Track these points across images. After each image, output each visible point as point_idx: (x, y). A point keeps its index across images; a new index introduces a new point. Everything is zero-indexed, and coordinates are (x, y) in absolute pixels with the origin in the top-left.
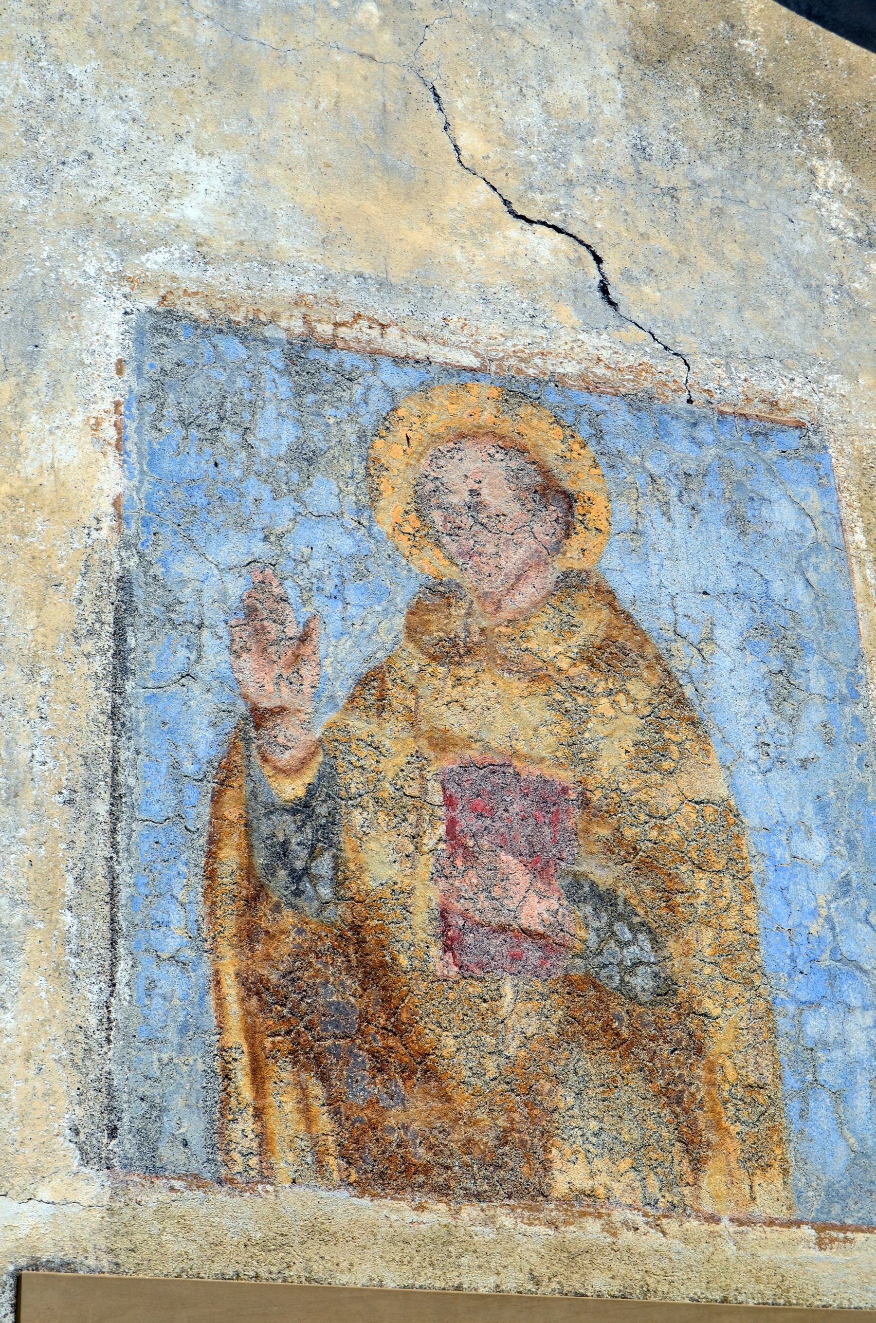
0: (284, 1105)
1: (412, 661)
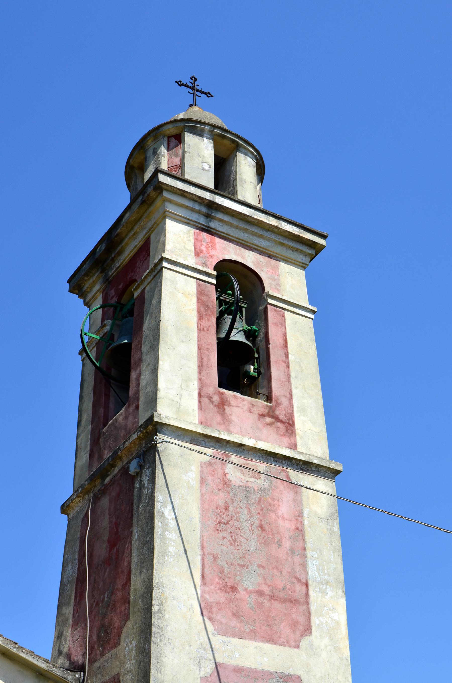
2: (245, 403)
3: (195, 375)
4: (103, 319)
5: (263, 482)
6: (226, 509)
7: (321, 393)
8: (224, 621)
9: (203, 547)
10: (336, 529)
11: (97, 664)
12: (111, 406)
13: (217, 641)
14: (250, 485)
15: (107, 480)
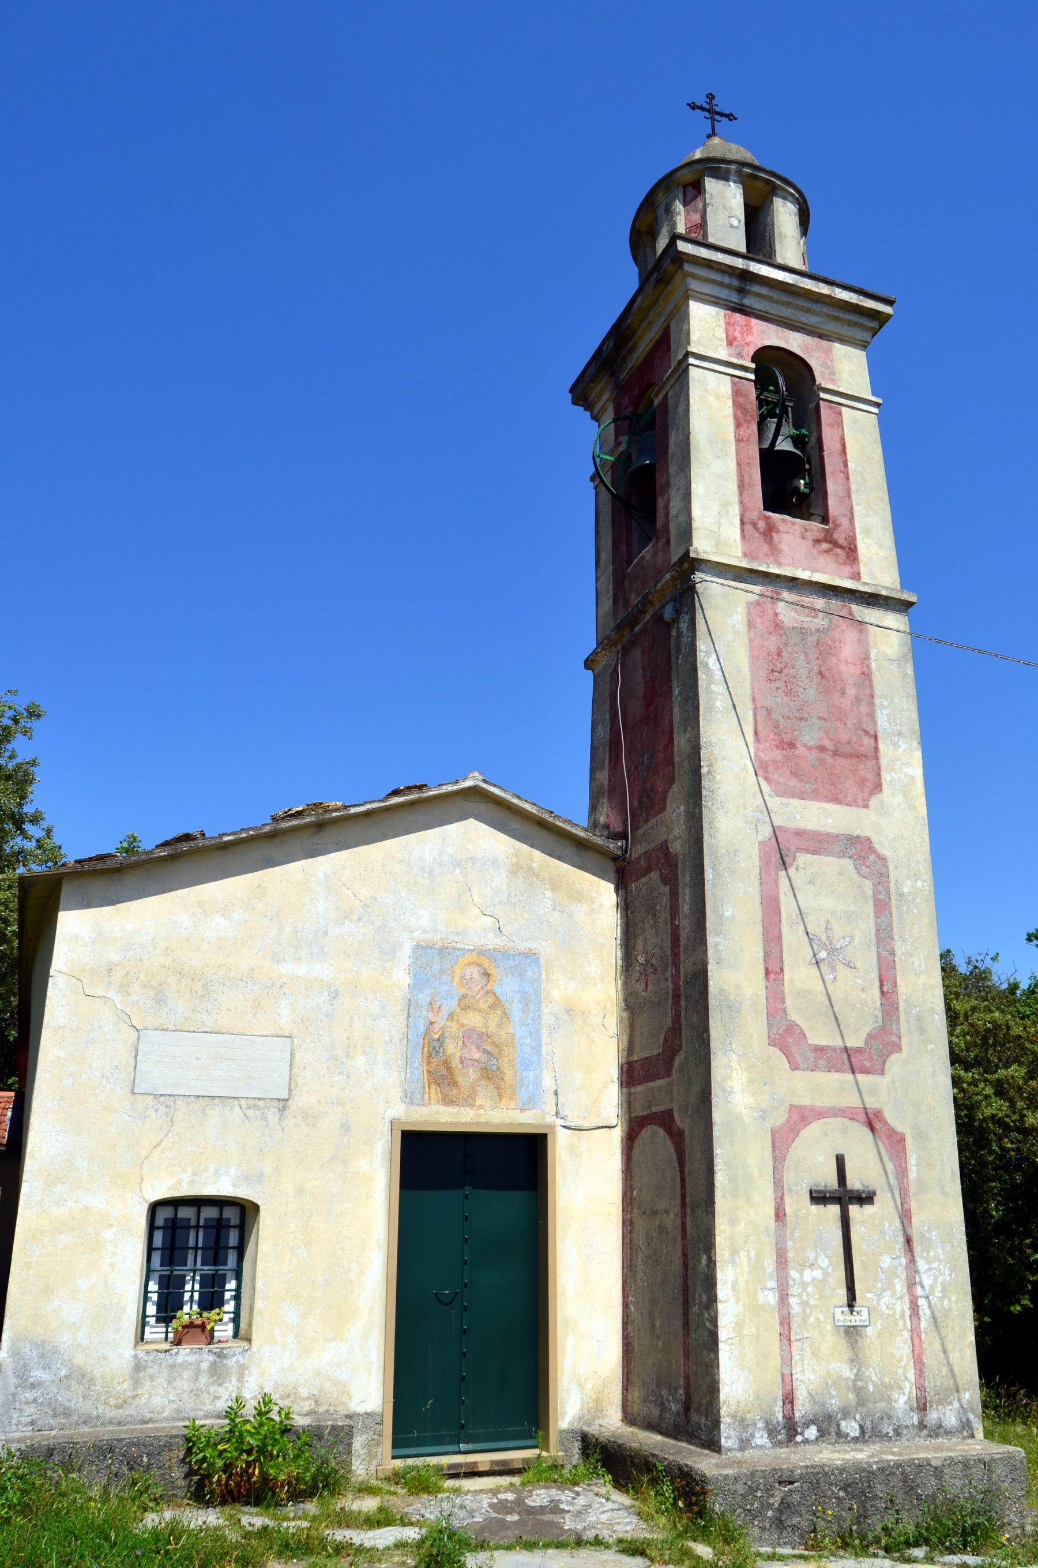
0: (433, 1091)
1: (459, 1010)
2: (797, 527)
3: (735, 498)
4: (617, 436)
5: (821, 622)
6: (779, 655)
7: (888, 508)
8: (782, 781)
9: (754, 700)
10: (910, 671)
11: (641, 832)
12: (635, 541)
13: (774, 802)
14: (806, 625)
15: (637, 629)
